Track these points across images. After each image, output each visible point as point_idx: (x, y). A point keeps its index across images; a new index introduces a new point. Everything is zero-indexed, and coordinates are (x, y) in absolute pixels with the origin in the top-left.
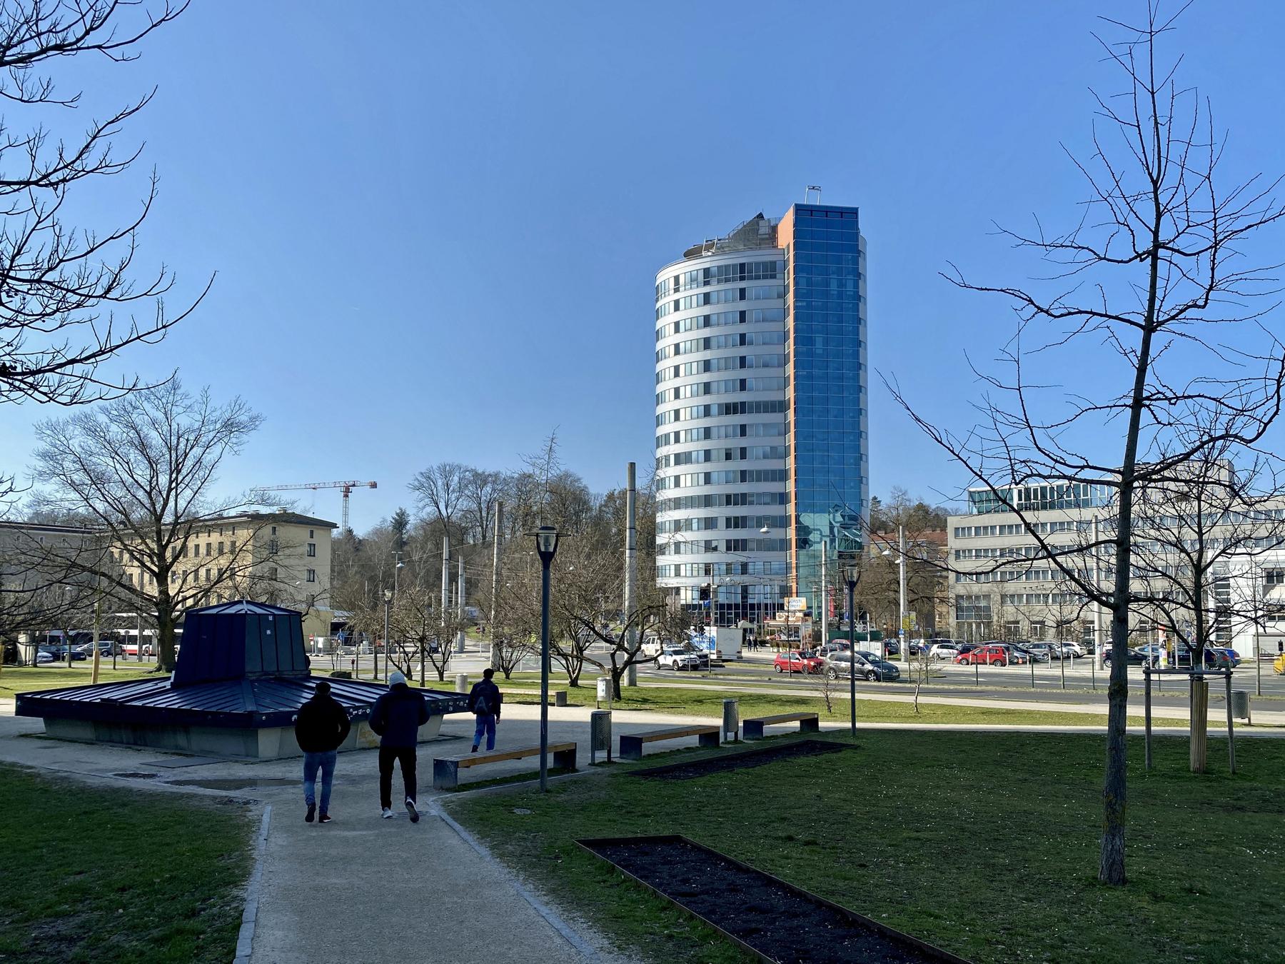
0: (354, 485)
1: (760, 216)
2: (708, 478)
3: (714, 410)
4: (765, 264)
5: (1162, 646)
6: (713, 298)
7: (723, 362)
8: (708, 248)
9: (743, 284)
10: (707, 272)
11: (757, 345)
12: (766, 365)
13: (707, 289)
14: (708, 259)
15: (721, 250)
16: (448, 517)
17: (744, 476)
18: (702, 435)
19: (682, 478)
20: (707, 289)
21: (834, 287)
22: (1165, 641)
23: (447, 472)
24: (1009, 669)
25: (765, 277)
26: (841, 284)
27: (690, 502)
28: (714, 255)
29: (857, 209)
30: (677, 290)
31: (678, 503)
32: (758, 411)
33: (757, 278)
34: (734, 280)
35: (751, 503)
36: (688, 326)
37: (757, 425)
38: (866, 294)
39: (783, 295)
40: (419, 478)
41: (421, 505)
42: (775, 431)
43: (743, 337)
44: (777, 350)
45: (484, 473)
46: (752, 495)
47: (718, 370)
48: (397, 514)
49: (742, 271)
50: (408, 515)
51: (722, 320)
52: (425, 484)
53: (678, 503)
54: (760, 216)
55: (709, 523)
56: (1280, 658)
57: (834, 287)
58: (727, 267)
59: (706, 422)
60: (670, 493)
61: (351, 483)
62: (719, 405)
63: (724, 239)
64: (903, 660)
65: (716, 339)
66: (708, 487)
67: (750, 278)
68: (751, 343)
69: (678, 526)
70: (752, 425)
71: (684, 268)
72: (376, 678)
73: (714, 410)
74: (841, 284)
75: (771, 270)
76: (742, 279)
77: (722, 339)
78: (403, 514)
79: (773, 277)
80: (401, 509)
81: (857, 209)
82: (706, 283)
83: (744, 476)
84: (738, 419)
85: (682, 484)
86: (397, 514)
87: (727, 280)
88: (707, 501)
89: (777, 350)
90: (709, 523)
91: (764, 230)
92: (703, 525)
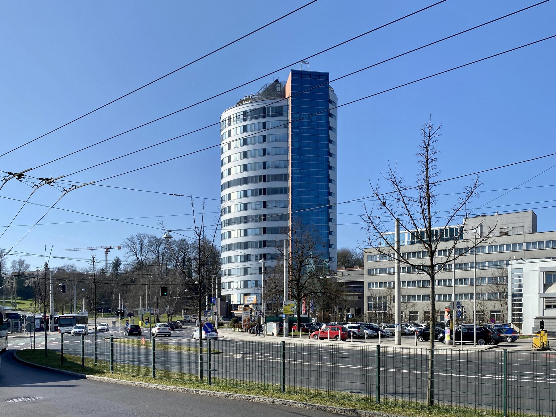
0: (110, 248)
1: (277, 81)
2: (246, 232)
3: (249, 193)
4: (277, 108)
5: (447, 325)
6: (249, 128)
7: (253, 165)
8: (246, 100)
9: (264, 120)
10: (245, 113)
11: (272, 155)
12: (277, 167)
13: (245, 123)
14: (246, 105)
15: (254, 101)
16: (142, 261)
17: (265, 231)
18: (242, 208)
19: (232, 233)
20: (245, 123)
21: (314, 120)
22: (449, 321)
23: (141, 238)
24: (352, 344)
25: (277, 116)
26: (319, 118)
27: (237, 246)
28: (249, 103)
29: (328, 74)
30: (229, 125)
31: (230, 247)
32: (273, 193)
33: (273, 116)
34: (260, 117)
35: (269, 246)
36: (253, 155)
37: (272, 201)
38: (336, 126)
39: (286, 126)
40: (126, 241)
41: (127, 255)
42: (282, 205)
43: (264, 151)
44: (283, 158)
45: (160, 238)
46: (269, 241)
47: (251, 170)
48: (115, 260)
49: (264, 112)
50: (121, 261)
51: (253, 142)
52: (131, 244)
53: (230, 247)
54: (277, 81)
55: (246, 258)
56: (538, 335)
57: (314, 120)
58: (255, 110)
59: (245, 200)
60: (227, 242)
61: (109, 247)
62: (252, 190)
63: (256, 95)
64: (284, 336)
65: (250, 152)
66: (246, 237)
67: (269, 116)
68: (269, 154)
69: (229, 260)
70: (269, 201)
71: (233, 112)
72: (31, 348)
73: (249, 193)
74: (319, 118)
75: (280, 112)
76: (264, 117)
77: (253, 152)
78: (118, 260)
79: (282, 115)
80: (117, 257)
81: (328, 74)
82: (245, 120)
83: (265, 231)
84: (263, 198)
85: (232, 236)
86: (115, 260)
87: (256, 118)
88: (245, 245)
89: (283, 158)
90: (246, 258)
91: (278, 89)
92: (243, 260)
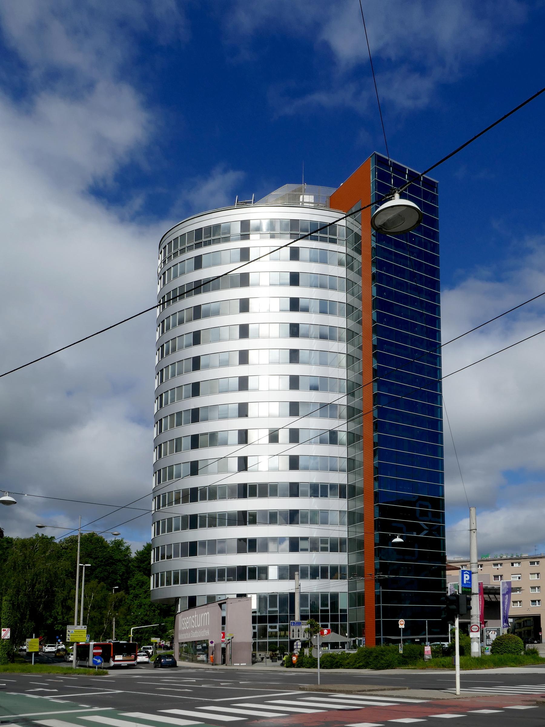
13: (244, 244)
20: (244, 244)
